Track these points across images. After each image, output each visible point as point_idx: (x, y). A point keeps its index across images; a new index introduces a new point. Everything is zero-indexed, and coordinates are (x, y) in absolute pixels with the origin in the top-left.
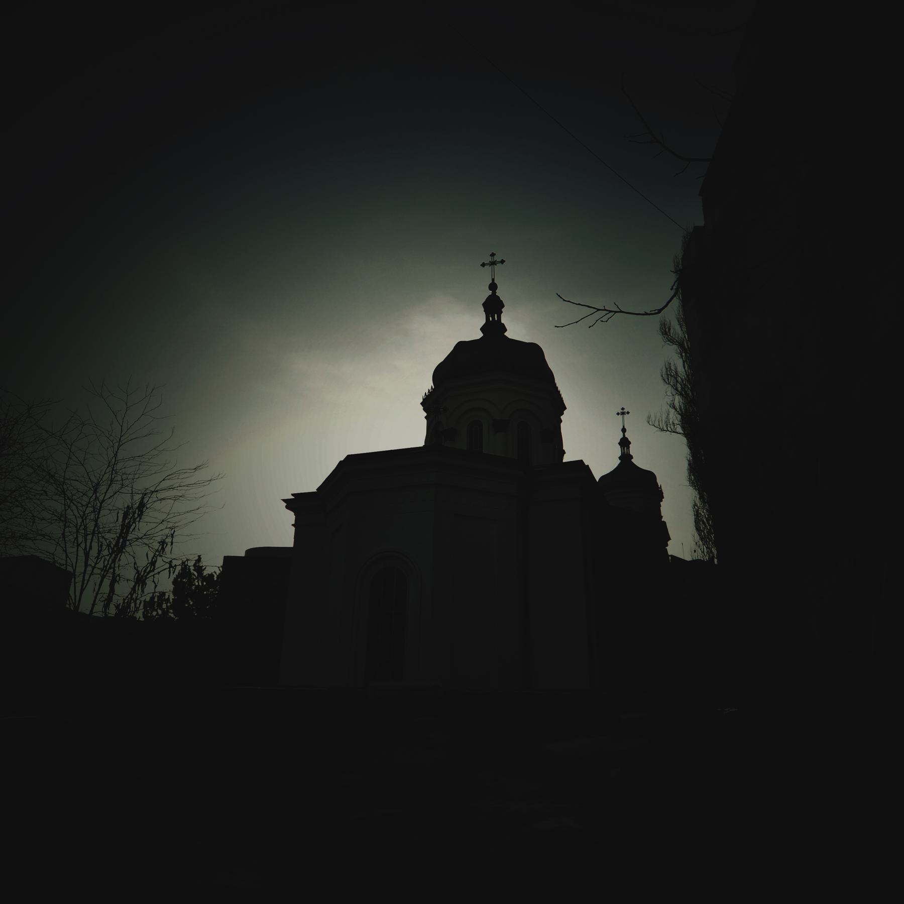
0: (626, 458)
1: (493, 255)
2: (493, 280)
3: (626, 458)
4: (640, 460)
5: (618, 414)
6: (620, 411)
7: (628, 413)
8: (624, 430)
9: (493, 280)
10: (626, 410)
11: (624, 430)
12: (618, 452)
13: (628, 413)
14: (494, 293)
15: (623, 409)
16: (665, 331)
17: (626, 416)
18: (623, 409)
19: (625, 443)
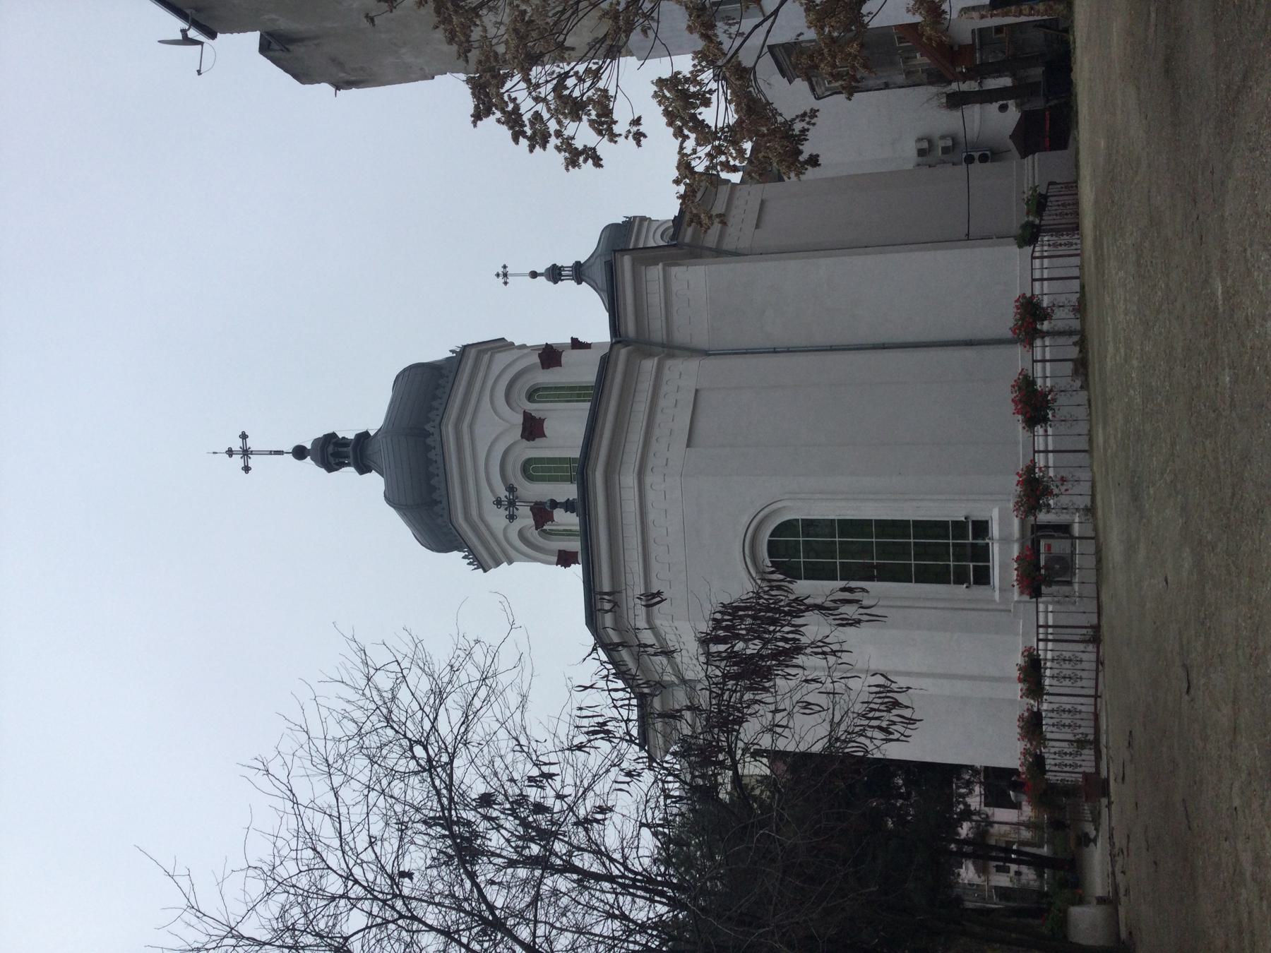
0: (579, 273)
1: (230, 452)
2: (300, 453)
3: (579, 273)
4: (583, 247)
5: (506, 283)
6: (501, 280)
7: (505, 267)
8: (534, 275)
9: (300, 453)
10: (501, 271)
11: (534, 275)
12: (568, 285)
13: (505, 267)
14: (541, 275)
15: (498, 275)
16: (498, 121)
17: (509, 270)
18: (498, 275)
19: (555, 274)
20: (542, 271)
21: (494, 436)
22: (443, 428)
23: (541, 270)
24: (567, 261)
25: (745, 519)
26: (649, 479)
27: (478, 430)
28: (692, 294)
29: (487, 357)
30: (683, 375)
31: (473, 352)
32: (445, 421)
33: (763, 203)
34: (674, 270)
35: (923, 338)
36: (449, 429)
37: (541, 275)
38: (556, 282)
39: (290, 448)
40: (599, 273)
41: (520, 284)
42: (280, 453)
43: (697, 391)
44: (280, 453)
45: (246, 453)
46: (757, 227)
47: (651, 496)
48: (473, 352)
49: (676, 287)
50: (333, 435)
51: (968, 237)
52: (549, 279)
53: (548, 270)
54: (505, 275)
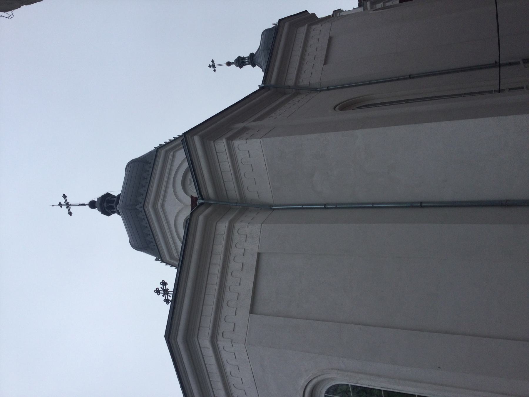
1: (60, 205)
5: (215, 70)
6: (212, 69)
8: (229, 64)
9: (92, 205)
11: (229, 64)
13: (213, 61)
14: (233, 63)
15: (210, 66)
18: (210, 66)
20: (232, 61)
21: (176, 212)
22: (145, 208)
23: (232, 61)
24: (246, 54)
25: (302, 382)
26: (221, 343)
27: (168, 207)
28: (253, 158)
29: (171, 154)
30: (250, 236)
31: (287, 25)
32: (146, 204)
33: (330, 39)
34: (236, 143)
35: (458, 198)
36: (150, 209)
37: (233, 63)
38: (241, 67)
39: (87, 202)
40: (262, 59)
41: (222, 70)
42: (83, 205)
43: (259, 254)
44: (83, 205)
45: (68, 205)
46: (325, 63)
47: (225, 356)
48: (162, 153)
49: (240, 155)
50: (108, 195)
51: (499, 91)
52: (237, 66)
53: (236, 60)
54: (214, 66)
